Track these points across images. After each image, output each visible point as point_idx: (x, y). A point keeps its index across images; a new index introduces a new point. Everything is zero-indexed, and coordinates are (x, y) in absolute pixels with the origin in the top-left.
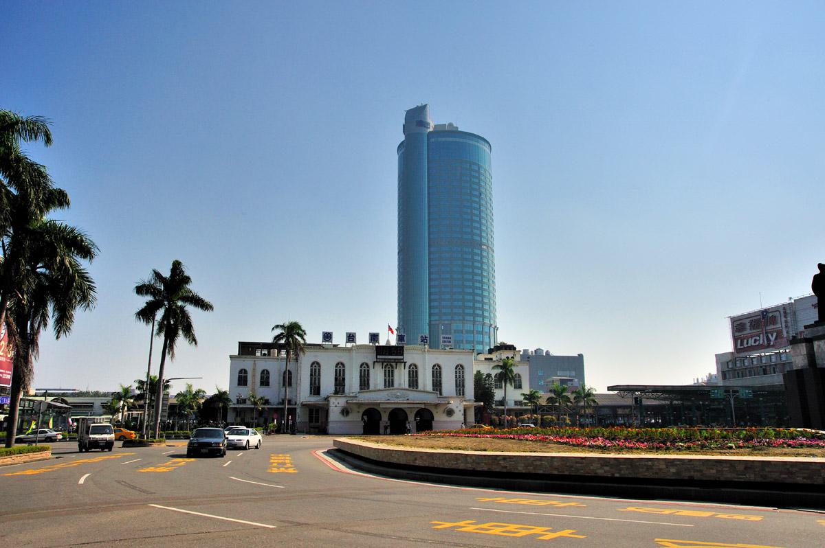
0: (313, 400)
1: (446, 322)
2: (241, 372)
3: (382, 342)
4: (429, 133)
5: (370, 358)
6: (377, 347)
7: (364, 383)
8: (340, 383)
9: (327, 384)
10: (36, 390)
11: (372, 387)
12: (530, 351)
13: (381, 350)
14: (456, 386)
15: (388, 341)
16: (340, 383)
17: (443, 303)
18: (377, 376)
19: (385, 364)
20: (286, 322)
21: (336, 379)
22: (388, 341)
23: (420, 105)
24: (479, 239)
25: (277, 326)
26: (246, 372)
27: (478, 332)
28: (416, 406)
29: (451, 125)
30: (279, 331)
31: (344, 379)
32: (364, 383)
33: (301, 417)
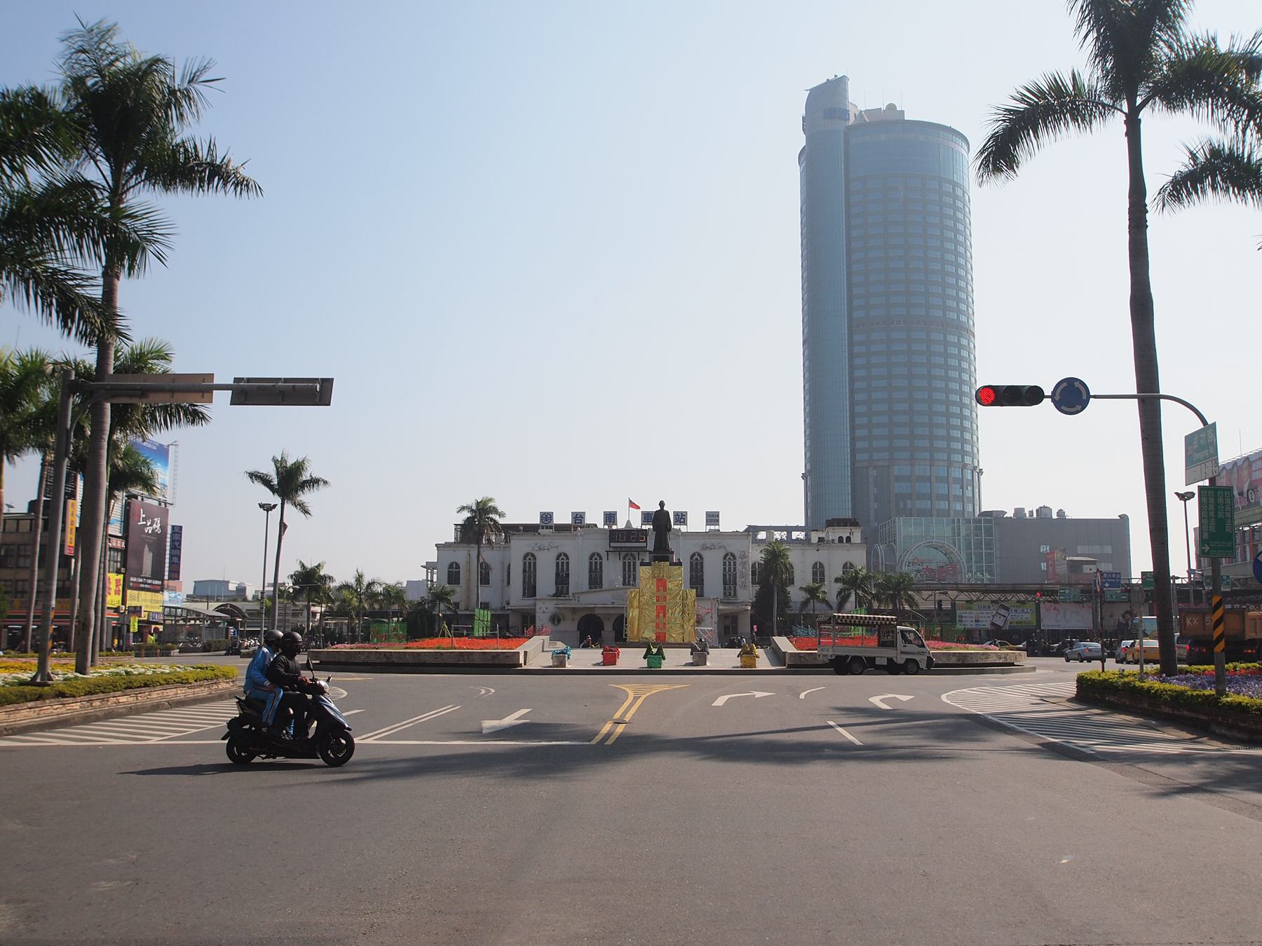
0: (527, 603)
1: (881, 463)
2: (451, 566)
3: (621, 524)
4: (849, 128)
5: (601, 546)
6: (612, 532)
7: (595, 580)
8: (562, 579)
9: (546, 580)
10: (526, 653)
11: (605, 586)
12: (1027, 512)
13: (615, 535)
14: (725, 583)
15: (628, 522)
16: (562, 579)
17: (876, 432)
18: (613, 570)
19: (623, 554)
20: (471, 502)
21: (557, 574)
22: (628, 522)
23: (831, 77)
24: (940, 313)
25: (463, 508)
26: (458, 566)
27: (940, 480)
28: (612, 612)
29: (891, 107)
30: (467, 514)
31: (568, 575)
32: (595, 580)
33: (923, 665)
